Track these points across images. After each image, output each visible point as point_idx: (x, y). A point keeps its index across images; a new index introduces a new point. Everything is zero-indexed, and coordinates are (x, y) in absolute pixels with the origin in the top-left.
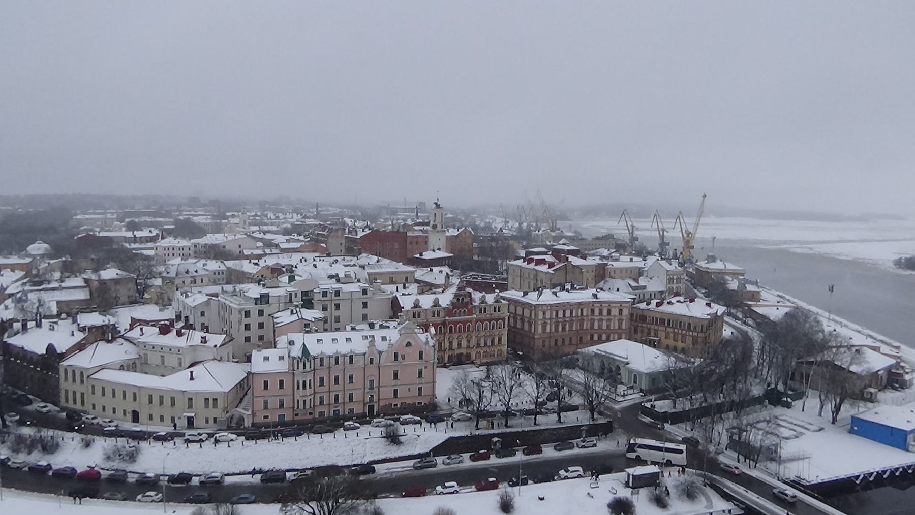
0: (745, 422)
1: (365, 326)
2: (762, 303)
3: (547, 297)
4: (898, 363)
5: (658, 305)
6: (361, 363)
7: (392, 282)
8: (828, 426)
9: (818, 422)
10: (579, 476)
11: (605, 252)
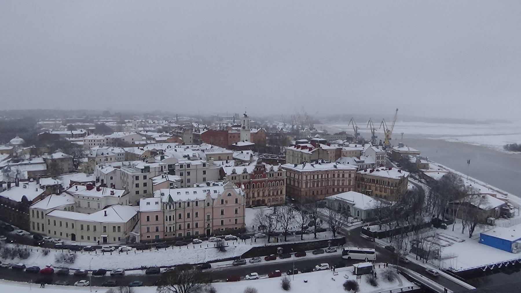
0: (420, 237)
1: (205, 184)
2: (430, 170)
3: (308, 167)
4: (506, 204)
6: (203, 206)
7: (220, 159)
8: (467, 239)
9: (461, 237)
10: (327, 269)
11: (341, 142)
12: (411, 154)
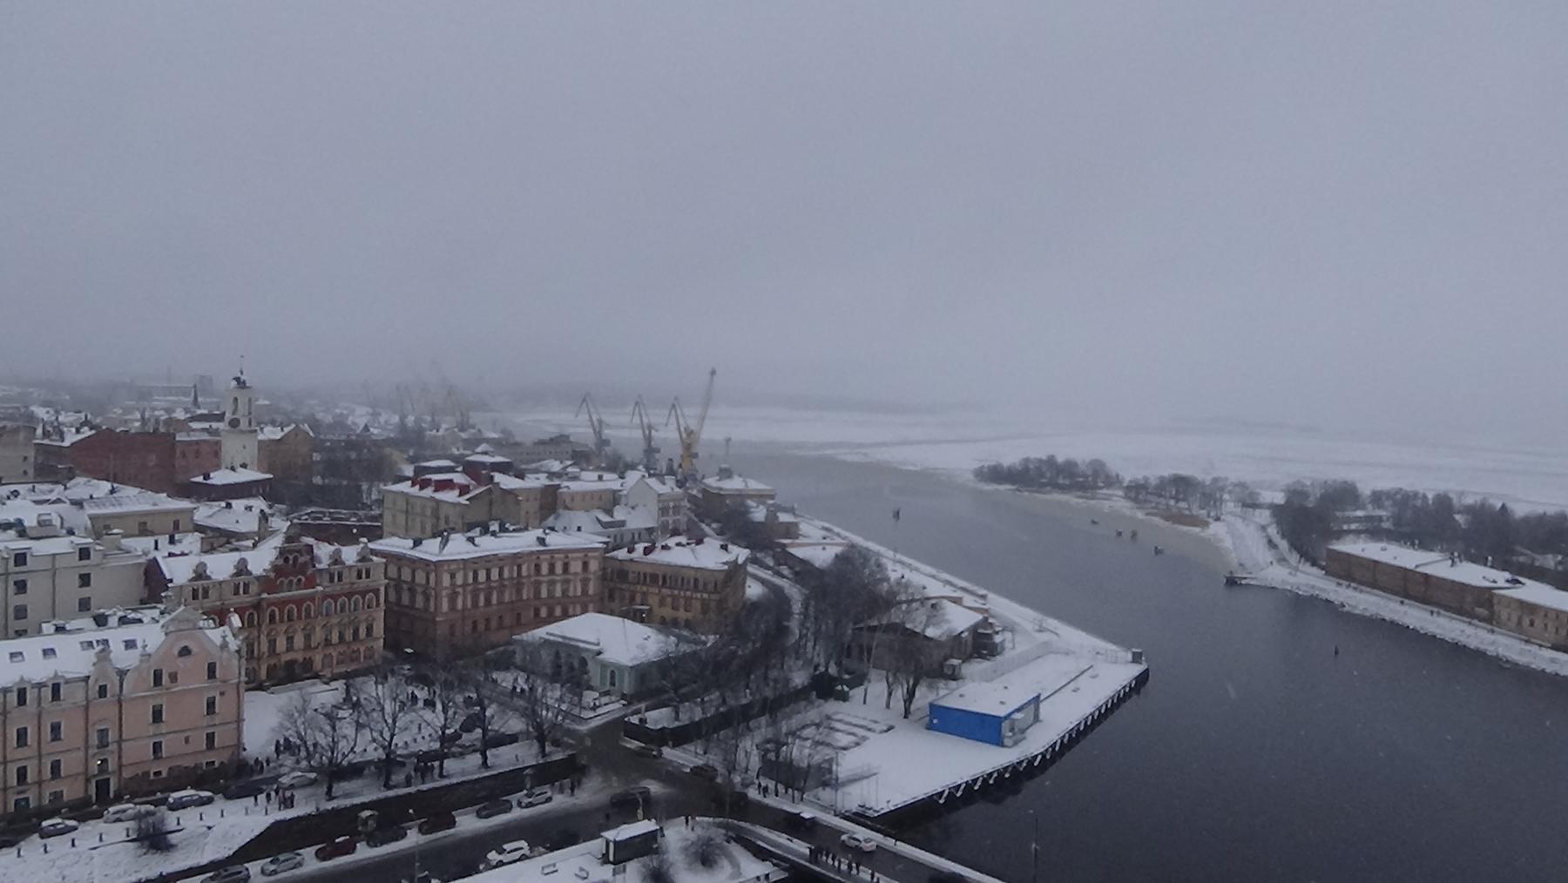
0: (784, 730)
1: (86, 622)
2: (801, 540)
3: (459, 547)
4: (986, 619)
5: (647, 551)
7: (144, 531)
11: (556, 466)
12: (751, 497)
